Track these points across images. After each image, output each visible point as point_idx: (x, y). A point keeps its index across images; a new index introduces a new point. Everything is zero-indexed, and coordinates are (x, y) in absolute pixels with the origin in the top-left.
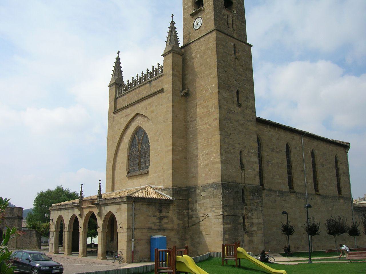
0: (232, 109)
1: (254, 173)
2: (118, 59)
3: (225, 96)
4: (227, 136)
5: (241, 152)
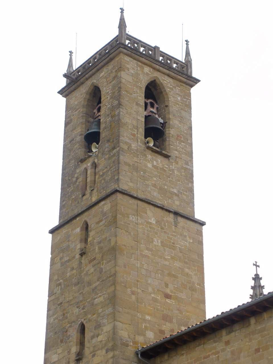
2: (257, 278)
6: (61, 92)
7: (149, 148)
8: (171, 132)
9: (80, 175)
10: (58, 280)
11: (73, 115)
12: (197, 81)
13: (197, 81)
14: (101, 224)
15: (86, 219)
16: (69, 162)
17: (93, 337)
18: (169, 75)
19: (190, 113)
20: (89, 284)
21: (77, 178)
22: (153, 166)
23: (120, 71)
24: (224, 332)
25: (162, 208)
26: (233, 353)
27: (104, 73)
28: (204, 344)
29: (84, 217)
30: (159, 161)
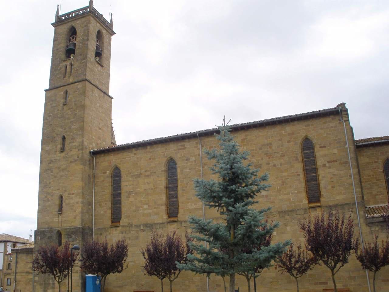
0: (53, 159)
1: (75, 214)
3: (48, 149)
4: (46, 186)
5: (61, 197)
6: (53, 24)
7: (97, 61)
8: (104, 55)
9: (63, 67)
10: (49, 113)
11: (59, 37)
12: (114, 33)
13: (114, 33)
14: (76, 93)
15: (67, 89)
16: (56, 59)
17: (70, 143)
18: (105, 29)
19: (110, 47)
20: (68, 119)
21: (61, 68)
22: (98, 70)
23: (89, 23)
24: (134, 150)
25: (100, 90)
26: (138, 158)
27: (79, 22)
28: (123, 153)
29: (66, 88)
30: (99, 68)
